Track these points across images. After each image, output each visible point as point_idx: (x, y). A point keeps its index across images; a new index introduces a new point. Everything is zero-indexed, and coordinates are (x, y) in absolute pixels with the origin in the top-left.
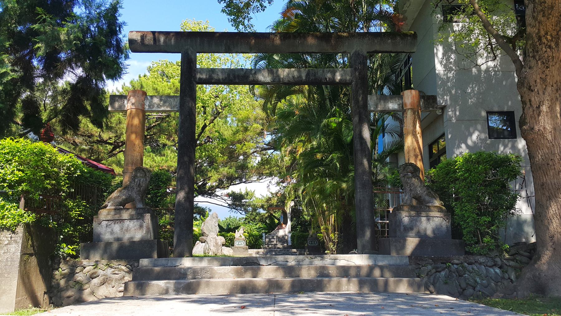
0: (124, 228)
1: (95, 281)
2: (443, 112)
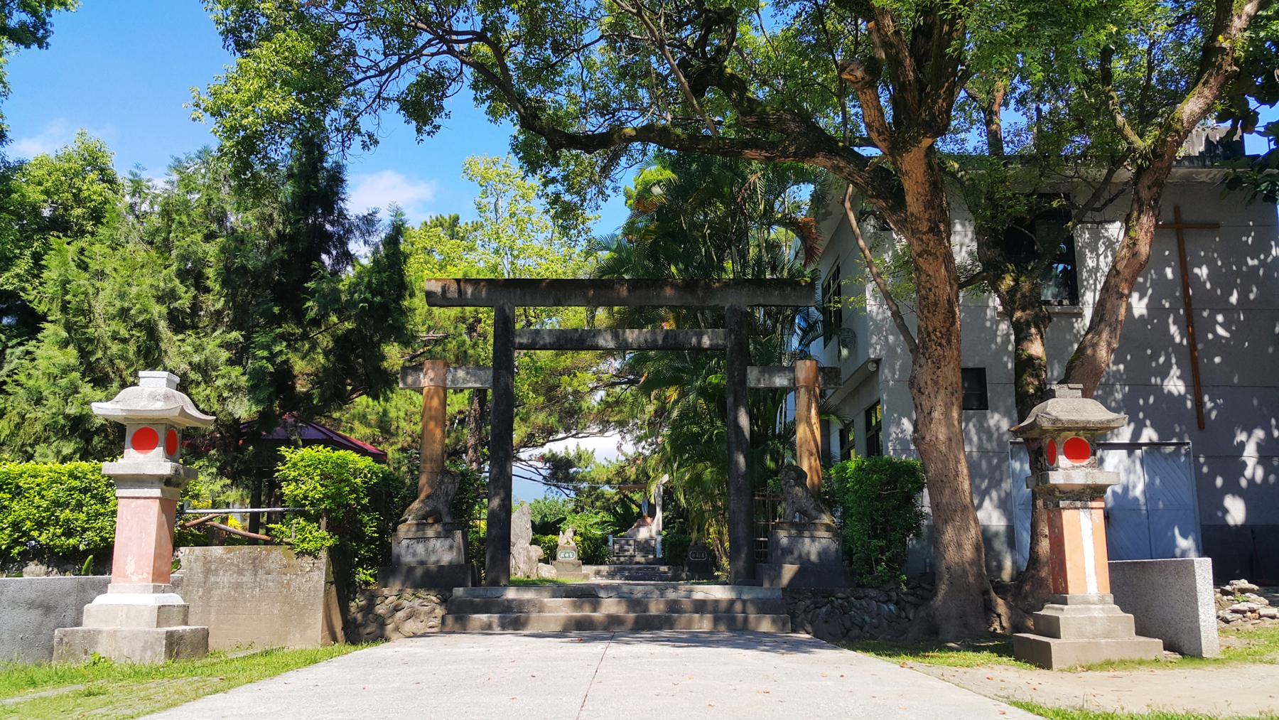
1: (400, 614)
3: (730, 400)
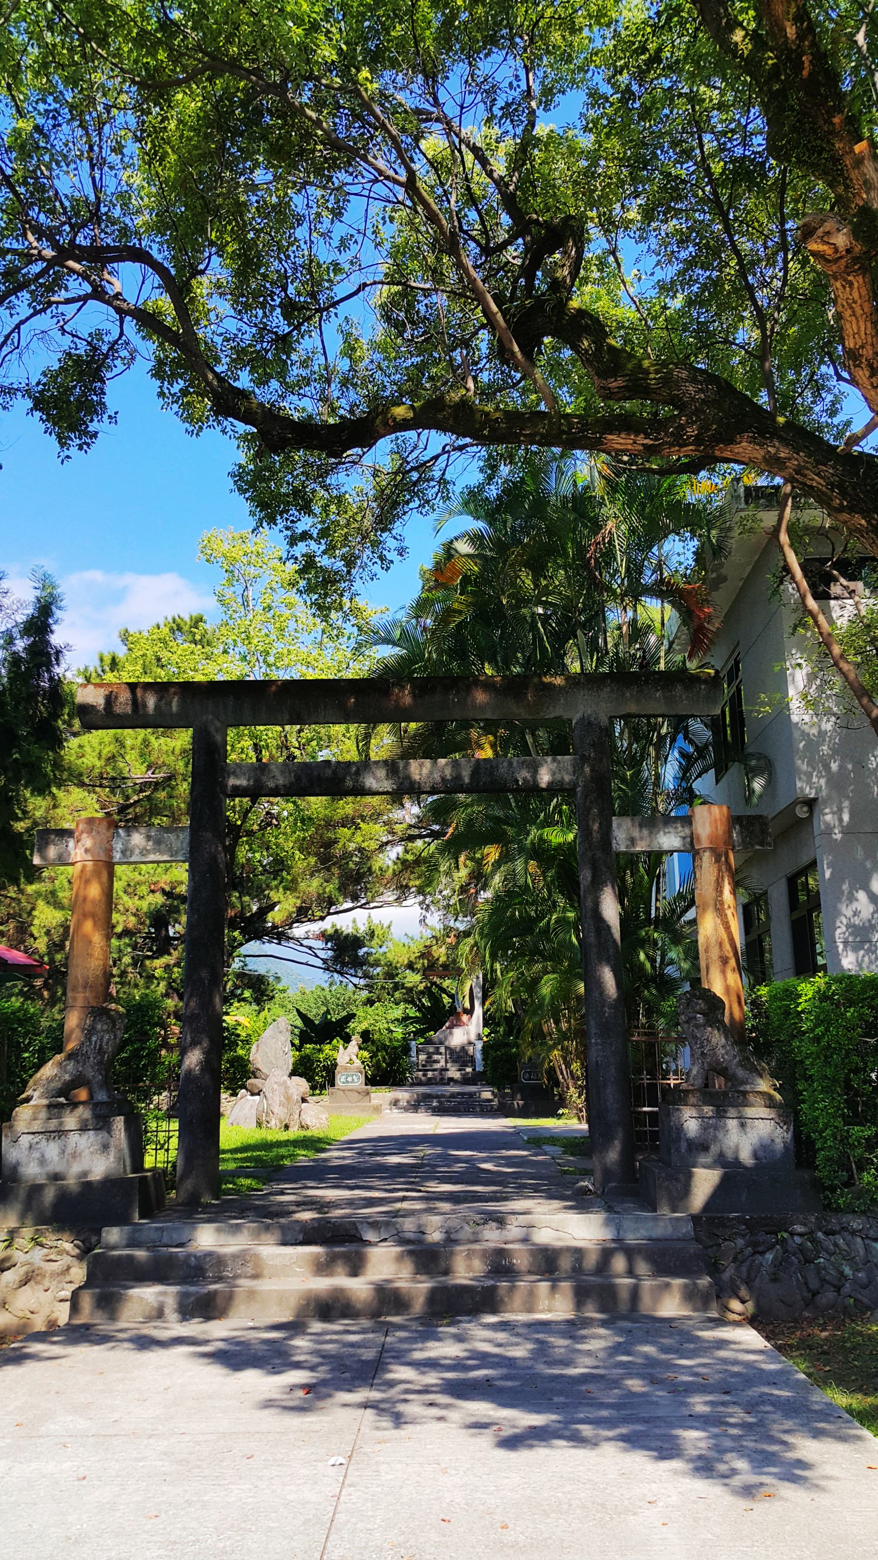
0: (69, 1150)
2: (811, 811)
3: (585, 876)
